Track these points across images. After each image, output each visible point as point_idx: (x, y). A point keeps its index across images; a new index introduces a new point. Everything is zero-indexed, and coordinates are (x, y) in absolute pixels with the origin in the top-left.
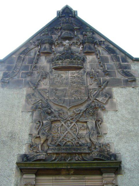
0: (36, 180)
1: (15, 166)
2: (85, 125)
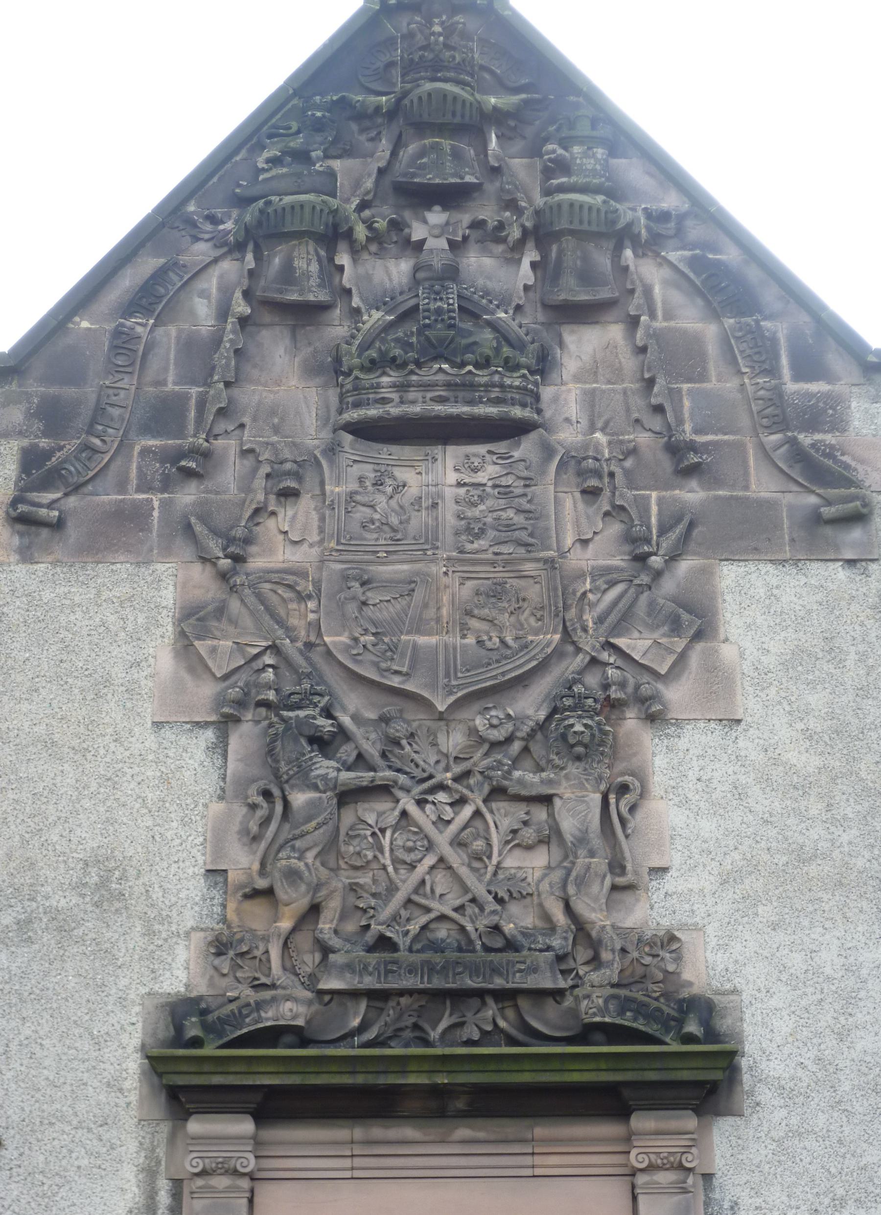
0: (258, 1142)
1: (134, 1064)
2: (540, 814)
